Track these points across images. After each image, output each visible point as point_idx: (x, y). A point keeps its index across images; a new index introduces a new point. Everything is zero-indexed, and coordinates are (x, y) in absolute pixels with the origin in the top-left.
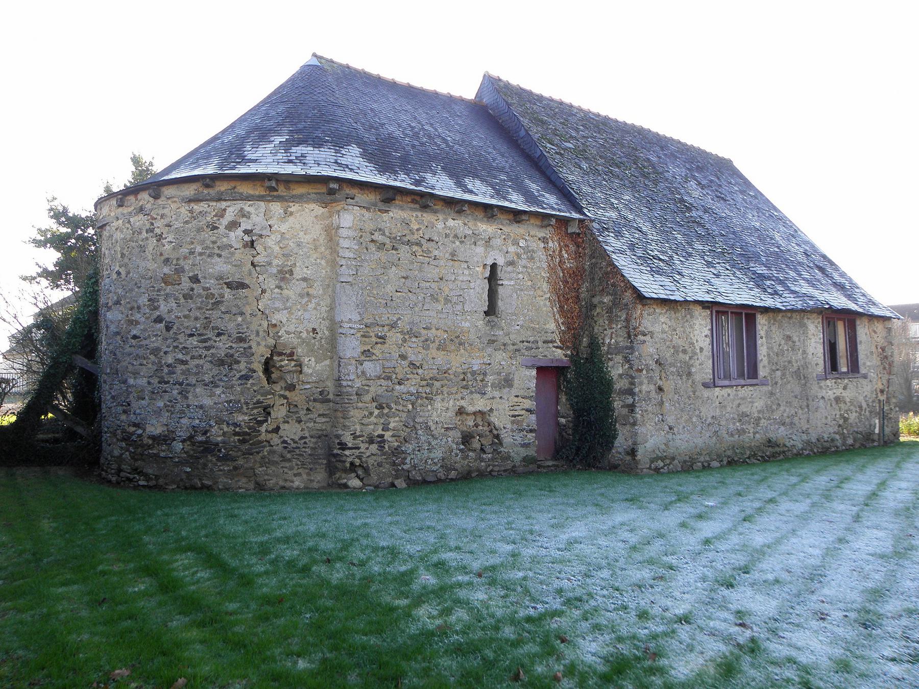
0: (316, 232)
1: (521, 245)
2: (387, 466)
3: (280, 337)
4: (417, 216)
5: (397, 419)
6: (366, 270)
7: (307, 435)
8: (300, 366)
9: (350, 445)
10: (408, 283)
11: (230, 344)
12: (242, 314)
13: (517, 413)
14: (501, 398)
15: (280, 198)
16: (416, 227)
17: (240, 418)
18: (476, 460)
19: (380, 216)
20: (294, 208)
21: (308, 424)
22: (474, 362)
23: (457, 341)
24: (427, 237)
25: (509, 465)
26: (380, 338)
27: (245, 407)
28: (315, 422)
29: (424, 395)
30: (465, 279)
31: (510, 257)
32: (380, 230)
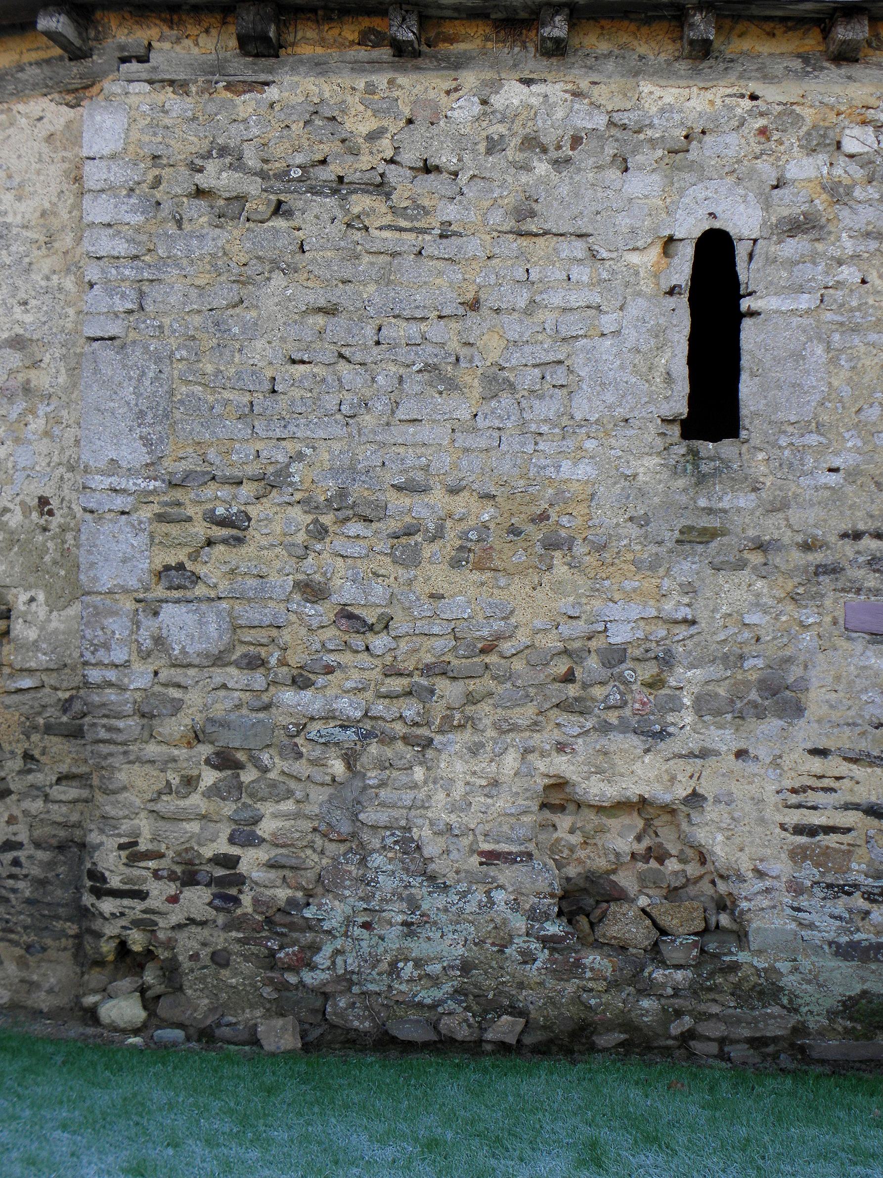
1: (850, 146)
2: (248, 967)
4: (371, 89)
5: (288, 806)
6: (172, 294)
7: (23, 837)
9: (115, 882)
10: (337, 327)
13: (817, 819)
14: (741, 754)
16: (364, 128)
18: (614, 985)
19: (224, 105)
21: (26, 804)
22: (614, 611)
23: (536, 533)
24: (409, 157)
25: (774, 1022)
26: (223, 522)
28: (46, 798)
29: (399, 728)
30: (576, 299)
31: (789, 204)
32: (223, 151)
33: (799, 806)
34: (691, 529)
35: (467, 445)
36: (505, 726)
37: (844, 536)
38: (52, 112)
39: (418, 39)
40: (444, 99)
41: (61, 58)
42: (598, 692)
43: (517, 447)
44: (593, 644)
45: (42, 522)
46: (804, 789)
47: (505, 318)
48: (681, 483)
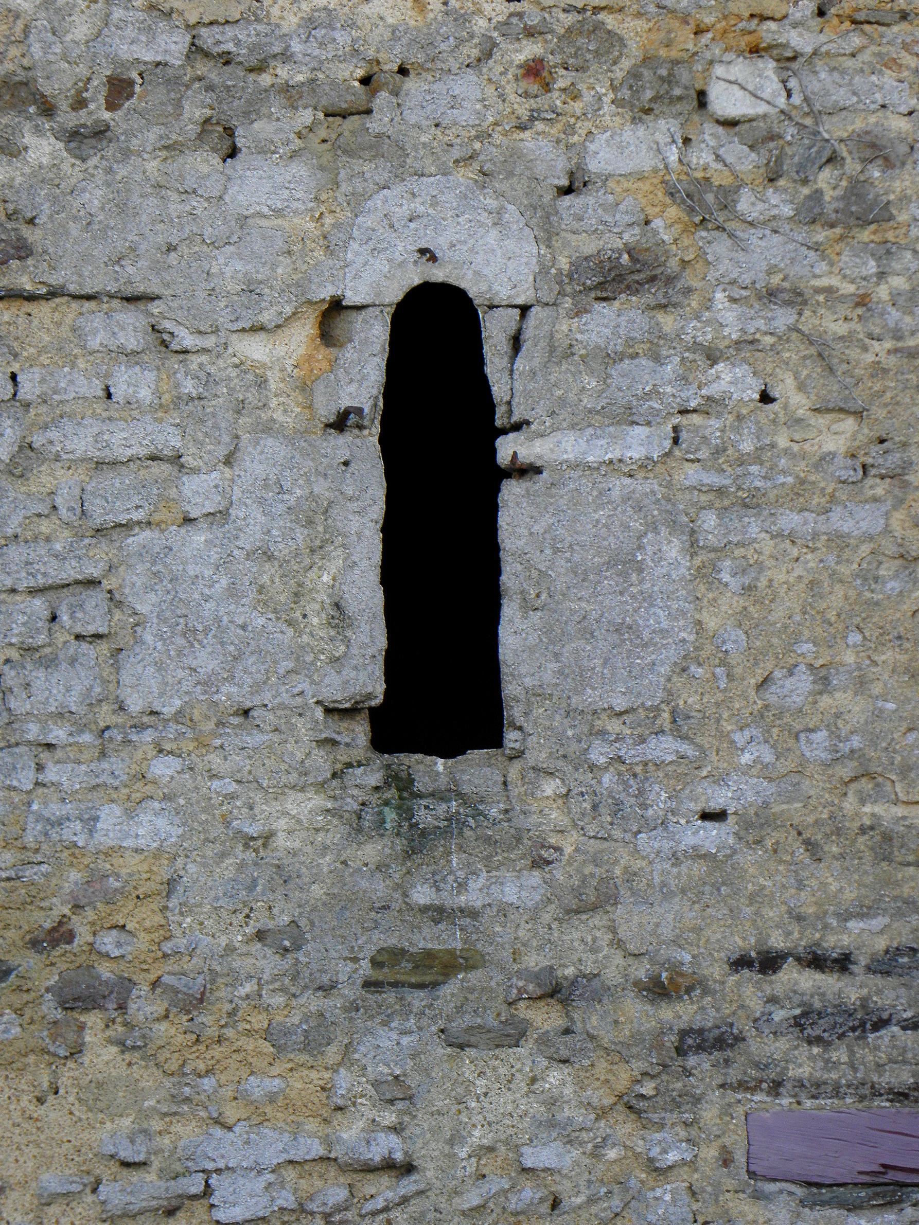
0: (777, 103)
1: (727, 101)
22: (226, 1148)
30: (125, 440)
31: (597, 228)
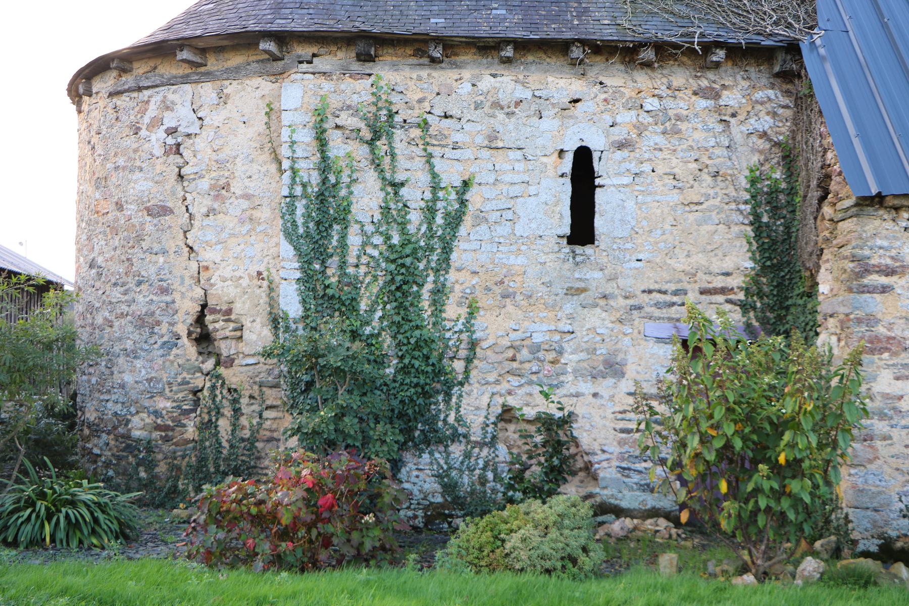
3: (212, 285)
8: (241, 329)
11: (151, 297)
12: (164, 252)
14: (595, 395)
15: (209, 76)
16: (416, 97)
17: (163, 404)
20: (231, 88)
23: (498, 290)
24: (438, 111)
27: (167, 390)
30: (517, 178)
31: (619, 134)
32: (349, 107)
33: (622, 419)
34: (571, 288)
35: (465, 248)
36: (483, 382)
37: (644, 291)
38: (265, 86)
39: (442, 56)
40: (455, 83)
41: (268, 60)
42: (527, 366)
43: (489, 249)
44: (525, 343)
45: (259, 283)
46: (624, 412)
47: (482, 187)
48: (567, 266)
